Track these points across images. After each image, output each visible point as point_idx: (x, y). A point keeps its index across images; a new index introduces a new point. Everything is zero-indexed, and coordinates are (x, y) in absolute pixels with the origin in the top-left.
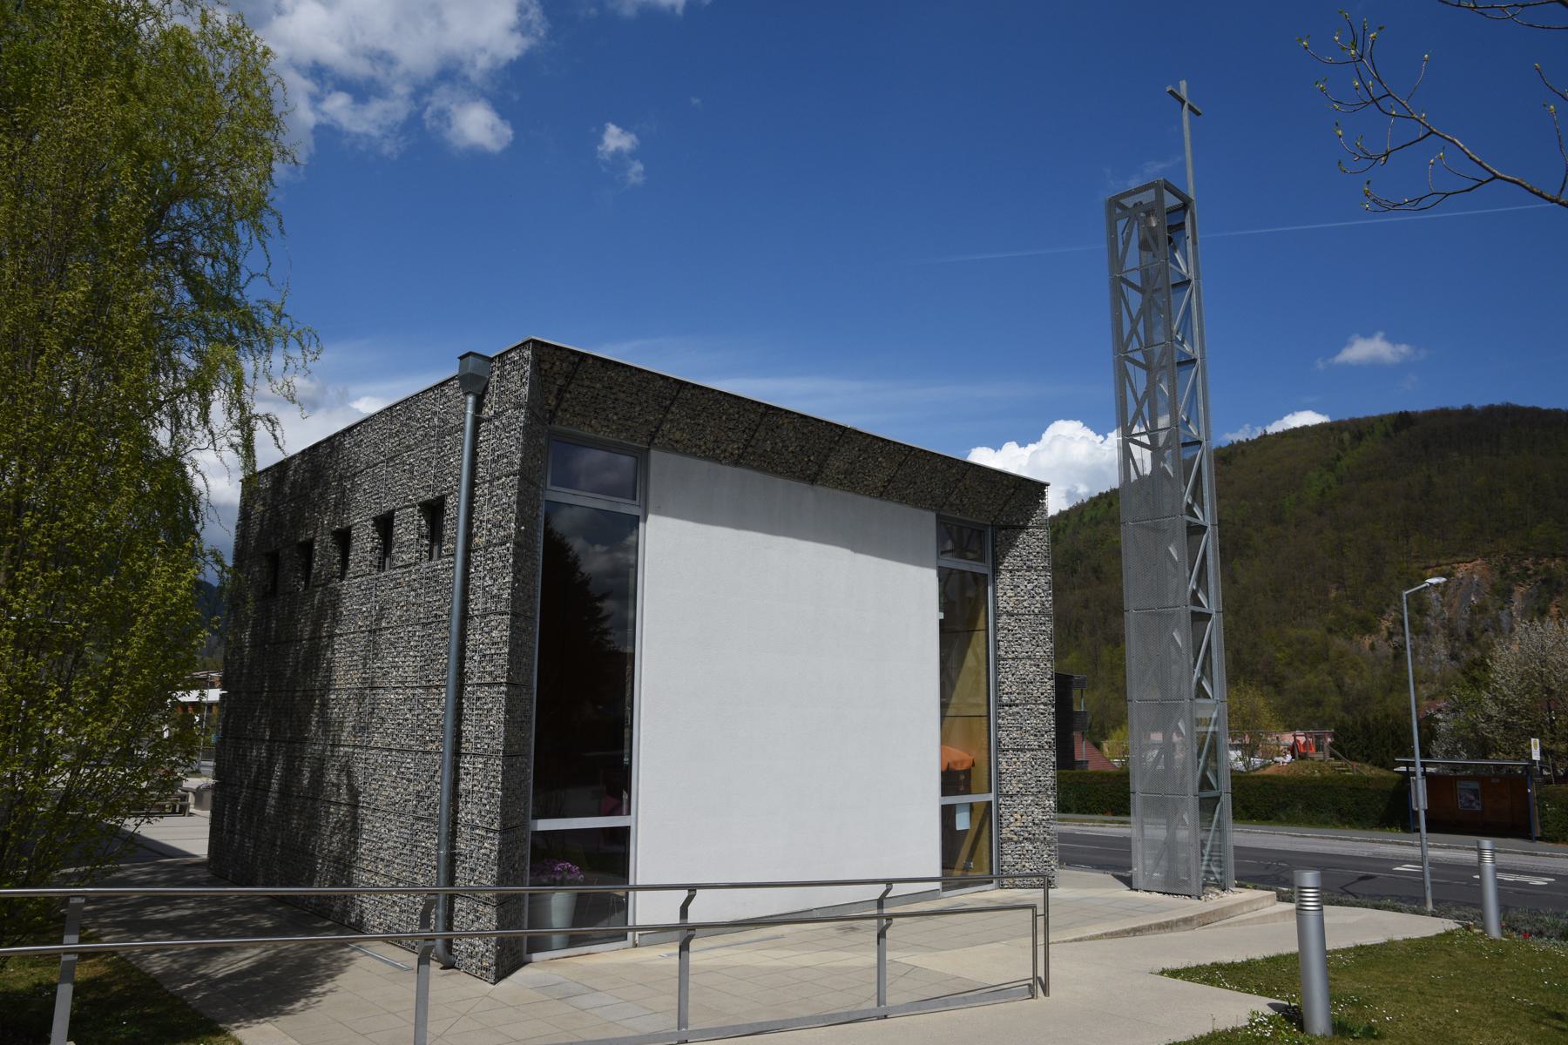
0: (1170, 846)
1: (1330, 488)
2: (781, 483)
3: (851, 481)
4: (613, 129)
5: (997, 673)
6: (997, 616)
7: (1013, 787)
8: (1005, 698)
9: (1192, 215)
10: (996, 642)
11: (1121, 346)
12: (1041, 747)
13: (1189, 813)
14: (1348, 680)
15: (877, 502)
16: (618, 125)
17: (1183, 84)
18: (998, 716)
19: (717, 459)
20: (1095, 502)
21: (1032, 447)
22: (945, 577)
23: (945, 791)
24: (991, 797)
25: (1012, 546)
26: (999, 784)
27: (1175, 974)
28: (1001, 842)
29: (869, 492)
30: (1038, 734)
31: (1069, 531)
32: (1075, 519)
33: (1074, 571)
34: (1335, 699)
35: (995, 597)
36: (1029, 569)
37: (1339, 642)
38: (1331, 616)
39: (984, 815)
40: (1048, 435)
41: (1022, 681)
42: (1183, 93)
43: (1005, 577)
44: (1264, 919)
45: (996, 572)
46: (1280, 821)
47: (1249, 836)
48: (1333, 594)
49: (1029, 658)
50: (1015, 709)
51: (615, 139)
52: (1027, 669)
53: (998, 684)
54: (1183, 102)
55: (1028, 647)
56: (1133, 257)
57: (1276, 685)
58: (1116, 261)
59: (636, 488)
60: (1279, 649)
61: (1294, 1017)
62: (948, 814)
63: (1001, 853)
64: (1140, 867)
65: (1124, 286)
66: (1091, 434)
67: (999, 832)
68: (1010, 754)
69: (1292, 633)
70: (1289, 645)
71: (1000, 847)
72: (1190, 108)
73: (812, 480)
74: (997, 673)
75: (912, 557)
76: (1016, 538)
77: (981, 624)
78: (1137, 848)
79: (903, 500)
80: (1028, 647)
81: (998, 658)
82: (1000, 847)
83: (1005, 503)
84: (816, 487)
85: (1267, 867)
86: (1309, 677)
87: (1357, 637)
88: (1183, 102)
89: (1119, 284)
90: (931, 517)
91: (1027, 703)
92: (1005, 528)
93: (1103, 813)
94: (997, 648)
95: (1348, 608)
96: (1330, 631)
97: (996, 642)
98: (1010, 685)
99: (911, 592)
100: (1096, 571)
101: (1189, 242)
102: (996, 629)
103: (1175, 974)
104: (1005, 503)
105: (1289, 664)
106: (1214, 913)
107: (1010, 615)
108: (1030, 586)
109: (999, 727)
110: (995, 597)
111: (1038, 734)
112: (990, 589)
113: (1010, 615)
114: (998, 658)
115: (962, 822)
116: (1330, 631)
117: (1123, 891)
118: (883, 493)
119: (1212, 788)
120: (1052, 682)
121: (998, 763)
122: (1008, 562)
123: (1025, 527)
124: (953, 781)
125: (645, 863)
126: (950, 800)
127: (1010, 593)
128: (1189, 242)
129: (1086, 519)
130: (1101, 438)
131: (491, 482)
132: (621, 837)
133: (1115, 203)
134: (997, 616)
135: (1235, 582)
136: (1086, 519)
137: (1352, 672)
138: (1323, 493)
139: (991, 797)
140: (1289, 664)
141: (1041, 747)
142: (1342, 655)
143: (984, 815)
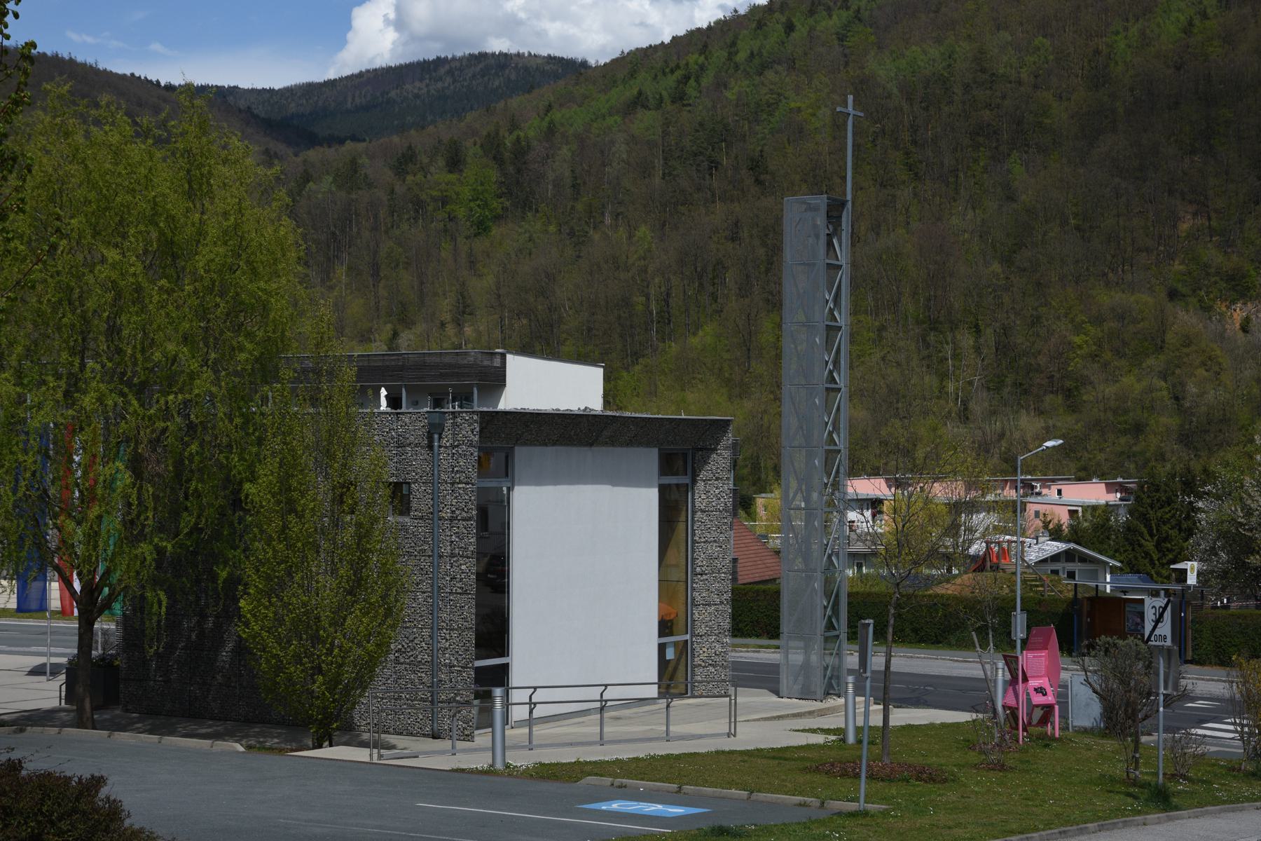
0: (806, 667)
1: (1204, 16)
2: (574, 450)
3: (613, 442)
5: (693, 552)
7: (702, 630)
8: (698, 569)
10: (693, 530)
12: (722, 603)
13: (818, 644)
14: (1192, 389)
18: (693, 582)
19: (546, 445)
22: (663, 490)
23: (662, 633)
24: (688, 637)
25: (706, 463)
26: (693, 628)
27: (803, 731)
28: (694, 667)
29: (621, 445)
30: (720, 593)
31: (707, 80)
32: (719, 55)
33: (714, 165)
34: (1169, 421)
35: (693, 499)
36: (717, 479)
37: (1185, 319)
38: (1178, 267)
39: (683, 648)
41: (711, 558)
43: (700, 485)
45: (694, 482)
46: (950, 646)
47: (915, 662)
48: (1184, 226)
52: (713, 549)
53: (693, 559)
55: (715, 534)
57: (1068, 394)
59: (507, 471)
60: (1078, 329)
61: (844, 740)
62: (662, 648)
63: (693, 674)
64: (785, 682)
67: (693, 660)
69: (1106, 298)
70: (1098, 320)
71: (693, 671)
73: (591, 445)
74: (693, 552)
75: (649, 486)
76: (709, 457)
77: (683, 518)
78: (783, 670)
79: (640, 444)
80: (715, 534)
81: (694, 542)
82: (693, 671)
84: (595, 449)
85: (914, 690)
86: (1128, 380)
87: (1220, 307)
92: (701, 449)
93: (758, 636)
94: (693, 535)
95: (1211, 254)
96: (1173, 295)
97: (693, 530)
98: (701, 560)
99: (644, 502)
100: (756, 166)
103: (803, 731)
105: (1094, 357)
106: (828, 709)
107: (703, 511)
109: (693, 589)
111: (720, 593)
113: (703, 511)
114: (694, 542)
115: (670, 654)
116: (1173, 295)
117: (774, 698)
118: (630, 443)
119: (834, 628)
121: (693, 614)
124: (665, 627)
125: (516, 678)
126: (664, 640)
127: (703, 496)
129: (741, 56)
131: (453, 484)
132: (505, 668)
134: (694, 513)
135: (1011, 198)
136: (741, 56)
137: (1201, 372)
138: (1188, 29)
139: (688, 637)
140: (1094, 357)
141: (722, 603)
142: (1187, 341)
143: (683, 648)
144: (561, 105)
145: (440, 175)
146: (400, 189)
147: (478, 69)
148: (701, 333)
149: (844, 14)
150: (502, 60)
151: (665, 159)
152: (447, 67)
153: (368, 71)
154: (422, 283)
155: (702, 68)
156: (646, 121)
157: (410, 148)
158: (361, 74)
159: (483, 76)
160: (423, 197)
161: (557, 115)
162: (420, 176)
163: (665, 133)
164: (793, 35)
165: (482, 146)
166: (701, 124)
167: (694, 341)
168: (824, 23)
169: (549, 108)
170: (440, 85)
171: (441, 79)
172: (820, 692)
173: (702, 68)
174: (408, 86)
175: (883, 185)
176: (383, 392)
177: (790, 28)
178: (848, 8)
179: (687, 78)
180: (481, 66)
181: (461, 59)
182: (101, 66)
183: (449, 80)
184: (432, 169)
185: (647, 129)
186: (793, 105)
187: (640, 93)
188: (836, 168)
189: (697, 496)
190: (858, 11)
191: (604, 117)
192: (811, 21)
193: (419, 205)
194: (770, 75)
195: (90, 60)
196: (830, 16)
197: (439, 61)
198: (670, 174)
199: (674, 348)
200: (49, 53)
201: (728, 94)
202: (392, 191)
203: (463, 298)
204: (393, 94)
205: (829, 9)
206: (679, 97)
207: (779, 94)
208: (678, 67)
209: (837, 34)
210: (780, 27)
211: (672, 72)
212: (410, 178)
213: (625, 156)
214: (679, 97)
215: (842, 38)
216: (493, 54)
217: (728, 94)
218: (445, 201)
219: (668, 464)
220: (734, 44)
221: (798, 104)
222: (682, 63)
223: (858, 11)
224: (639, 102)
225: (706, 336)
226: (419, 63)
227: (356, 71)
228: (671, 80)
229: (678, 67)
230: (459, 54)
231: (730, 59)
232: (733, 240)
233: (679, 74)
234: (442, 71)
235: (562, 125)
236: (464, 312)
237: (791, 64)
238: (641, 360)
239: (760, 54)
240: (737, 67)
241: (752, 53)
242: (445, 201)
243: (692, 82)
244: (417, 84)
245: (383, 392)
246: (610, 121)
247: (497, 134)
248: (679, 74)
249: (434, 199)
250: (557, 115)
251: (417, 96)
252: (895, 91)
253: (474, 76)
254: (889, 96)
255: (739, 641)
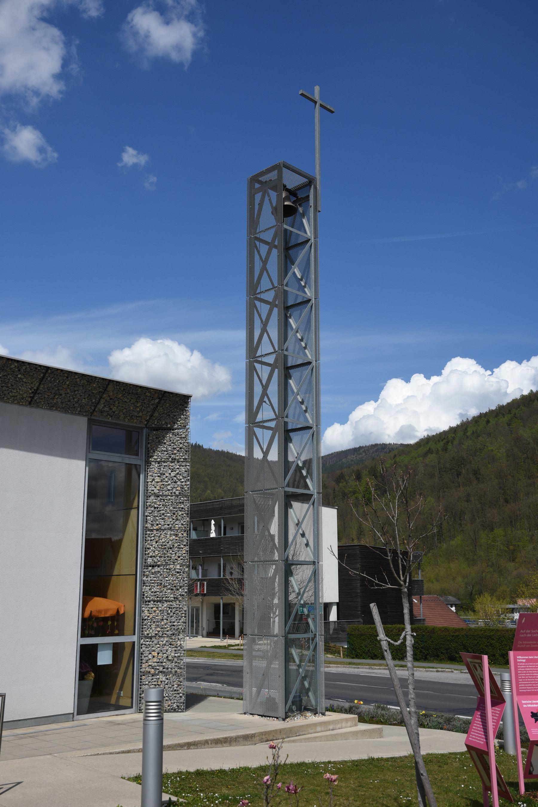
4: (131, 151)
6: (147, 497)
8: (150, 560)
9: (315, 188)
11: (253, 288)
12: (176, 599)
15: (27, 410)
16: (134, 148)
17: (317, 89)
20: (476, 420)
21: (435, 379)
24: (135, 638)
25: (160, 443)
26: (142, 629)
29: (18, 401)
30: (174, 588)
31: (456, 442)
33: (459, 474)
35: (146, 483)
40: (446, 371)
42: (317, 97)
43: (154, 467)
44: (345, 736)
45: (148, 463)
49: (170, 529)
50: (156, 569)
51: (130, 157)
52: (168, 538)
54: (316, 103)
56: (268, 220)
58: (253, 222)
65: (257, 243)
66: (482, 370)
68: (151, 605)
72: (321, 106)
76: (164, 437)
77: (135, 504)
79: (52, 407)
83: (154, 410)
88: (316, 103)
89: (253, 242)
90: (82, 422)
91: (167, 564)
92: (157, 429)
98: (154, 549)
100: (476, 473)
101: (312, 210)
102: (146, 507)
104: (154, 410)
108: (173, 474)
109: (144, 583)
110: (146, 483)
111: (174, 588)
112: (142, 477)
114: (145, 529)
115: (104, 658)
120: (187, 548)
121: (142, 611)
122: (157, 455)
123: (171, 429)
124: (91, 625)
127: (157, 479)
128: (312, 210)
129: (469, 433)
130: (489, 372)
133: (254, 179)
134: (147, 497)
139: (135, 638)
141: (176, 599)
144: (400, 455)
145: (353, 483)
146: (337, 489)
147: (375, 449)
148: (456, 539)
149: (510, 416)
150: (383, 446)
151: (439, 472)
152: (363, 449)
153: (335, 453)
154: (344, 523)
155: (454, 438)
156: (432, 458)
157: (342, 473)
158: (332, 454)
159: (376, 452)
160: (346, 491)
161: (398, 459)
162: (344, 484)
163: (439, 463)
164: (490, 424)
165: (369, 471)
166: (453, 458)
167: (453, 543)
168: (501, 420)
169: (395, 456)
170: (360, 456)
171: (361, 454)
172: (281, 712)
173: (454, 438)
174: (349, 457)
175: (529, 478)
176: (213, 522)
177: (488, 422)
178: (511, 414)
179: (448, 442)
180: (376, 448)
181: (368, 446)
182: (238, 454)
183: (364, 454)
184: (349, 481)
185: (432, 461)
186: (489, 448)
187: (430, 449)
188: (509, 472)
189: (150, 479)
190: (515, 414)
191: (416, 458)
192: (496, 419)
193: (344, 495)
194: (480, 438)
195: (234, 452)
196: (504, 417)
197: (360, 448)
198: (441, 477)
199: (444, 546)
200: (220, 450)
201: (464, 447)
202: (334, 490)
203: (360, 528)
204: (344, 460)
205: (503, 415)
206: (445, 449)
207: (484, 446)
208: (444, 439)
209: (507, 423)
210: (484, 423)
211: (442, 441)
212: (341, 484)
213: (423, 472)
214: (445, 449)
215: (509, 425)
216: (380, 444)
217: (464, 447)
218: (354, 493)
219: (95, 443)
220: (466, 429)
221: (492, 448)
222: (446, 437)
223: (515, 414)
224: (430, 451)
225: (458, 540)
226: (353, 449)
227: (330, 453)
228: (442, 444)
229: (444, 439)
230: (368, 444)
231: (465, 433)
232: (467, 501)
233: (444, 441)
234: (361, 451)
235: (400, 462)
236: (360, 534)
237: (489, 435)
238: (431, 551)
239: (477, 432)
240: (467, 437)
241: (473, 432)
242: (354, 493)
243: (450, 443)
244: (352, 456)
245: (213, 522)
246: (418, 459)
247: (375, 466)
248: (444, 441)
249: (350, 492)
250: (398, 459)
251: (352, 460)
252: (531, 441)
253: (373, 452)
254: (529, 444)
255: (417, 664)
